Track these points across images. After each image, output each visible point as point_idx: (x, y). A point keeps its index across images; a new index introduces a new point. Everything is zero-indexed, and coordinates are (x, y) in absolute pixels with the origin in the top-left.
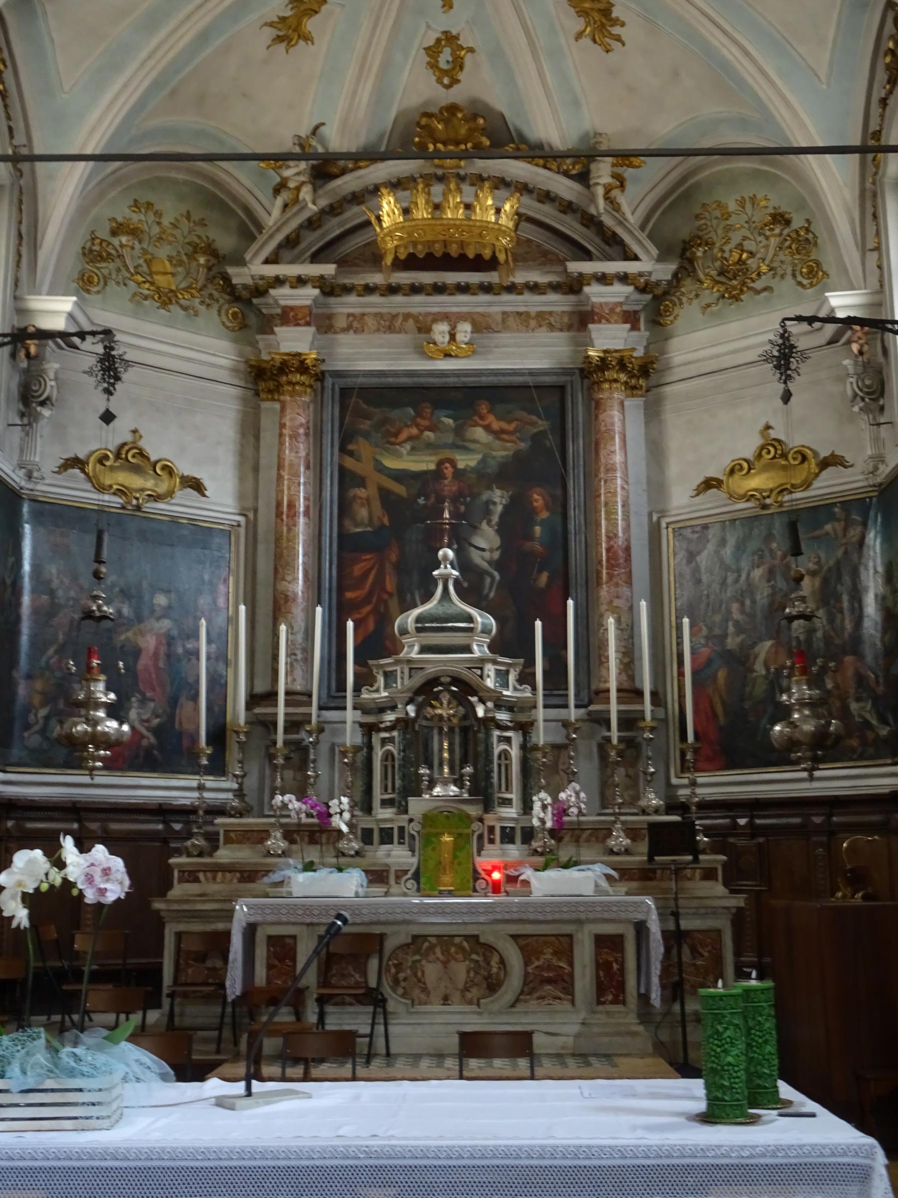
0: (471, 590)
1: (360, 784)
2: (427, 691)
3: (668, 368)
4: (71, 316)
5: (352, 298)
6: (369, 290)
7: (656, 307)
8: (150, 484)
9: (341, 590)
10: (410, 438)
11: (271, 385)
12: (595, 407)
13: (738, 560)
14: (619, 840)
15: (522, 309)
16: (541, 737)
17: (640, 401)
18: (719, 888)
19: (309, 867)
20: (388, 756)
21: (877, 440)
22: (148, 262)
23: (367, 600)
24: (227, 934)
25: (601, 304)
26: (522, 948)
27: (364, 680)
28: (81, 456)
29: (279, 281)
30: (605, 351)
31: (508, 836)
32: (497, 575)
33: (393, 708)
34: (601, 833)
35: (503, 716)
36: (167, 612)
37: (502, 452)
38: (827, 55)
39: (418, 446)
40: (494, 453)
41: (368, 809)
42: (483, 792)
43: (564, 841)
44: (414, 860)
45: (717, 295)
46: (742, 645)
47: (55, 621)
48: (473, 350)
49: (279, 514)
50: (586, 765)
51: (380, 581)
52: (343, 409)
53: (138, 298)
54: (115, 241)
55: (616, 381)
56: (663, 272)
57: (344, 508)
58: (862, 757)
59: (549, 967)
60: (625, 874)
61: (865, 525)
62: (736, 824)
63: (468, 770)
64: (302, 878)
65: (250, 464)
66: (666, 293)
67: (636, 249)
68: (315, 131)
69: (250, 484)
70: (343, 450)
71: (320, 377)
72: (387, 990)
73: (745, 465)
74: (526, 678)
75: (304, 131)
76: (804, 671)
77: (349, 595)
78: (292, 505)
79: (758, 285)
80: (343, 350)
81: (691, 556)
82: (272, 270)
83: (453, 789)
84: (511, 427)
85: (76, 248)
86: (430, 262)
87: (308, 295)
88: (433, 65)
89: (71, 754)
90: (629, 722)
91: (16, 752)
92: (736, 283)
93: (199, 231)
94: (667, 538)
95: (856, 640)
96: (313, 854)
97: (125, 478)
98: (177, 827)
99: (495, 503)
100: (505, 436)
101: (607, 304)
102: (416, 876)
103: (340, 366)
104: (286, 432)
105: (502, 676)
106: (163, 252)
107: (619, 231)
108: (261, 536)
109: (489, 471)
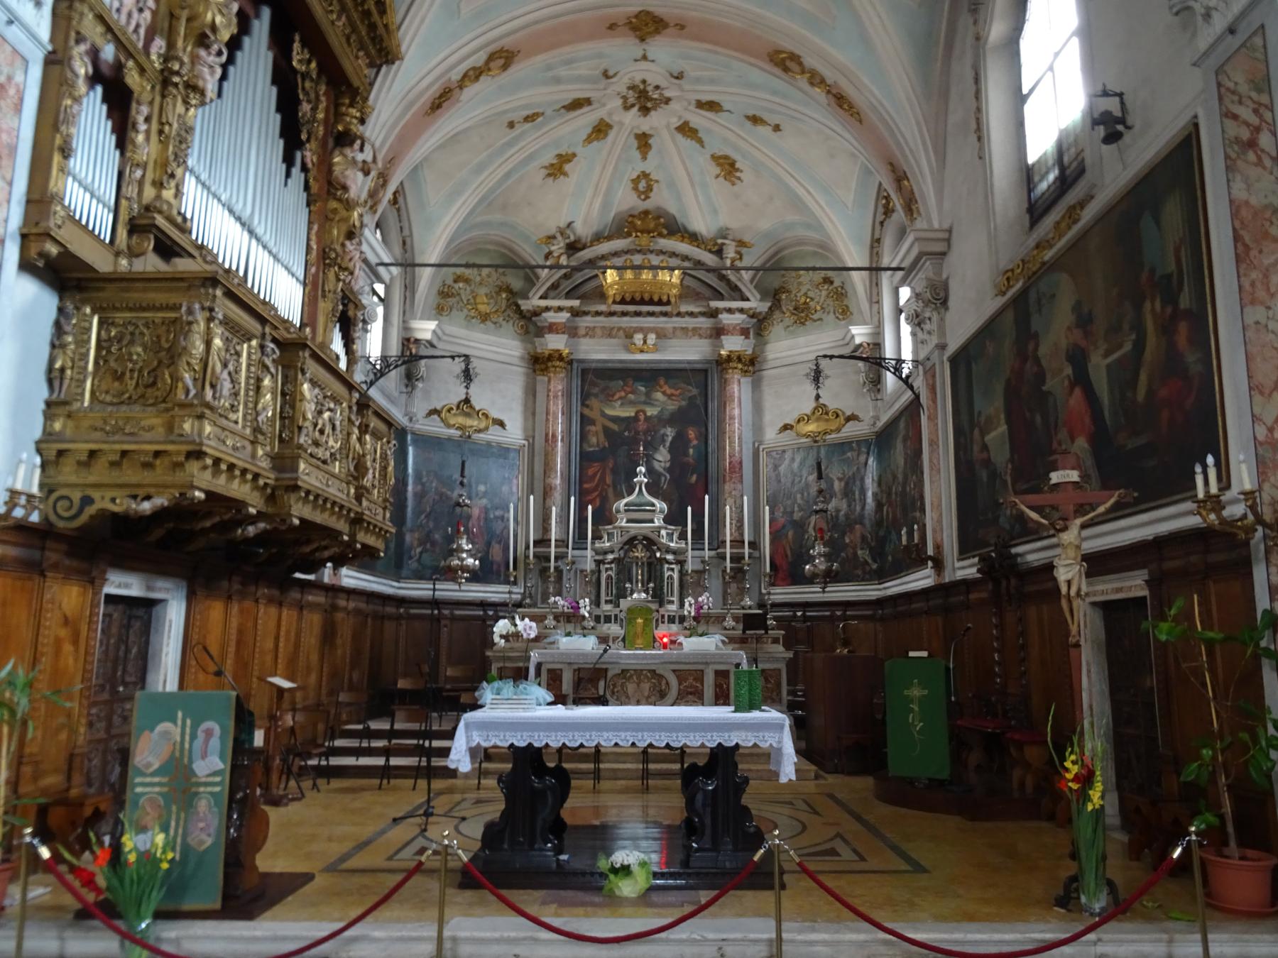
0: (653, 489)
1: (594, 592)
2: (631, 542)
3: (765, 361)
4: (434, 332)
5: (588, 318)
6: (598, 314)
7: (759, 326)
8: (475, 423)
9: (581, 482)
10: (621, 398)
11: (543, 366)
12: (724, 383)
13: (801, 471)
14: (729, 622)
16: (690, 567)
17: (749, 379)
18: (780, 648)
19: (568, 634)
20: (609, 577)
21: (875, 407)
22: (474, 298)
23: (595, 489)
24: (527, 669)
26: (678, 677)
27: (597, 537)
28: (438, 408)
29: (547, 309)
31: (671, 620)
33: (612, 552)
34: (720, 619)
35: (670, 557)
36: (485, 494)
37: (672, 406)
38: (852, 197)
39: (625, 403)
41: (598, 605)
42: (659, 597)
43: (700, 622)
44: (622, 632)
46: (801, 518)
47: (425, 500)
48: (656, 348)
49: (547, 440)
50: (714, 582)
51: (603, 479)
52: (583, 381)
53: (469, 318)
54: (456, 286)
56: (763, 307)
57: (583, 437)
58: (863, 580)
59: (691, 686)
60: (732, 640)
61: (868, 454)
62: (795, 616)
63: (651, 585)
64: (565, 640)
65: (530, 411)
66: (765, 318)
67: (748, 294)
68: (569, 225)
69: (530, 422)
70: (583, 404)
71: (571, 362)
72: (608, 697)
74: (683, 536)
75: (563, 224)
76: (822, 538)
77: (586, 486)
78: (554, 436)
79: (815, 317)
80: (583, 347)
81: (776, 467)
82: (544, 303)
83: (644, 595)
85: (435, 291)
86: (633, 302)
87: (565, 316)
88: (636, 189)
89: (450, 574)
90: (737, 559)
91: (404, 572)
92: (803, 315)
93: (503, 278)
94: (763, 457)
95: (862, 516)
96: (570, 627)
97: (461, 420)
98: (491, 613)
102: (624, 640)
103: (581, 356)
104: (551, 394)
105: (670, 536)
106: (483, 291)
107: (739, 284)
108: (537, 449)
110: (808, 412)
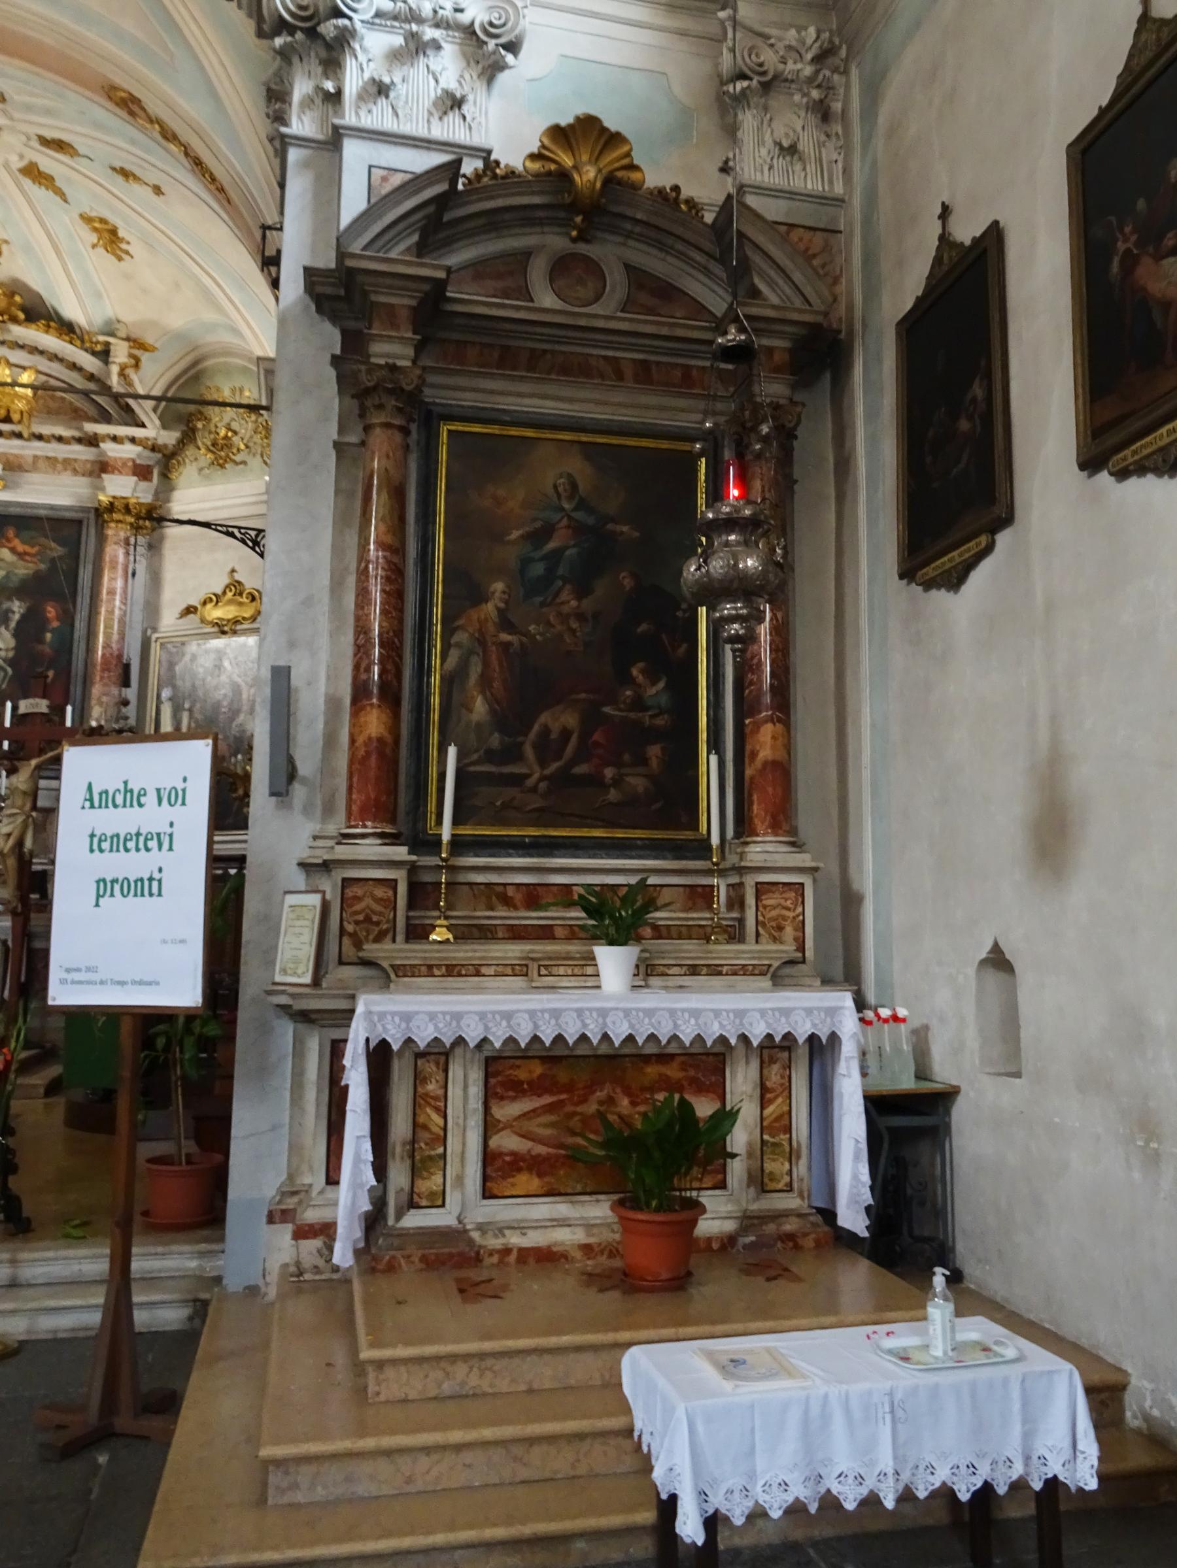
7: (162, 465)
15: (50, 454)
25: (115, 459)
30: (114, 497)
32: (9, 670)
40: (16, 571)
45: (209, 461)
55: (120, 521)
56: (169, 438)
73: (214, 598)
84: (34, 550)
99: (14, 612)
100: (27, 558)
101: (121, 458)
109: (11, 585)
110: (219, 591)
